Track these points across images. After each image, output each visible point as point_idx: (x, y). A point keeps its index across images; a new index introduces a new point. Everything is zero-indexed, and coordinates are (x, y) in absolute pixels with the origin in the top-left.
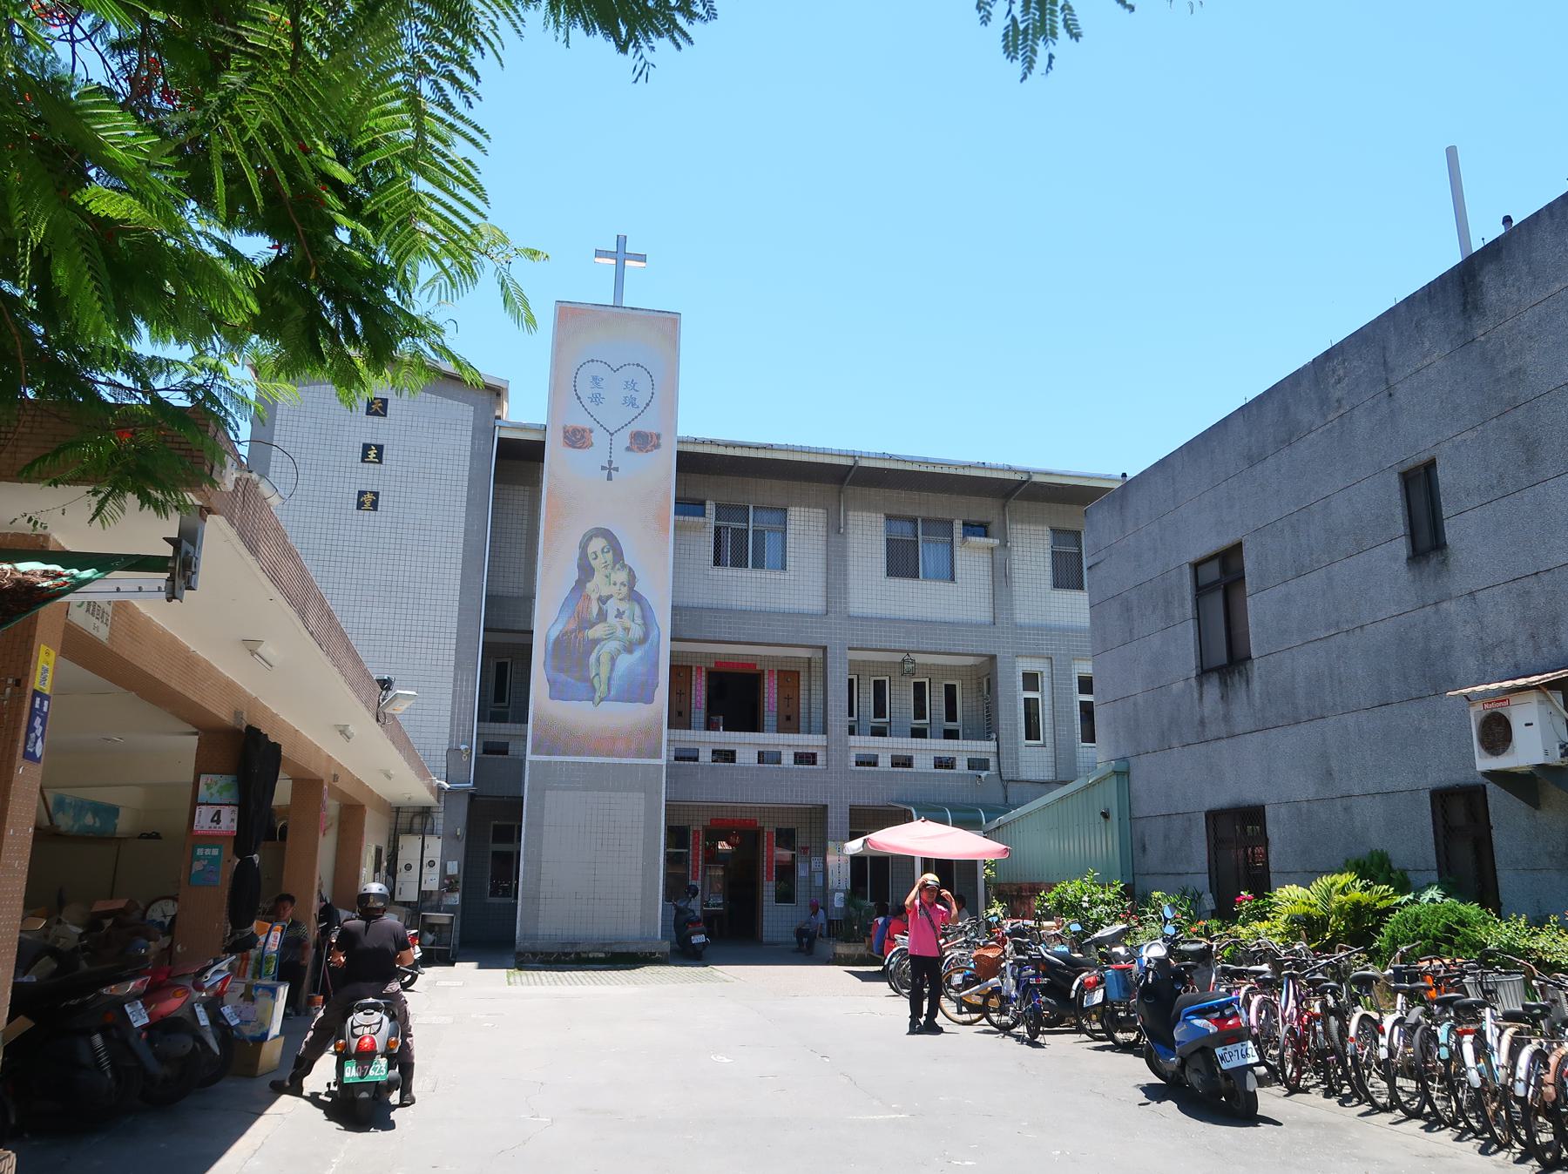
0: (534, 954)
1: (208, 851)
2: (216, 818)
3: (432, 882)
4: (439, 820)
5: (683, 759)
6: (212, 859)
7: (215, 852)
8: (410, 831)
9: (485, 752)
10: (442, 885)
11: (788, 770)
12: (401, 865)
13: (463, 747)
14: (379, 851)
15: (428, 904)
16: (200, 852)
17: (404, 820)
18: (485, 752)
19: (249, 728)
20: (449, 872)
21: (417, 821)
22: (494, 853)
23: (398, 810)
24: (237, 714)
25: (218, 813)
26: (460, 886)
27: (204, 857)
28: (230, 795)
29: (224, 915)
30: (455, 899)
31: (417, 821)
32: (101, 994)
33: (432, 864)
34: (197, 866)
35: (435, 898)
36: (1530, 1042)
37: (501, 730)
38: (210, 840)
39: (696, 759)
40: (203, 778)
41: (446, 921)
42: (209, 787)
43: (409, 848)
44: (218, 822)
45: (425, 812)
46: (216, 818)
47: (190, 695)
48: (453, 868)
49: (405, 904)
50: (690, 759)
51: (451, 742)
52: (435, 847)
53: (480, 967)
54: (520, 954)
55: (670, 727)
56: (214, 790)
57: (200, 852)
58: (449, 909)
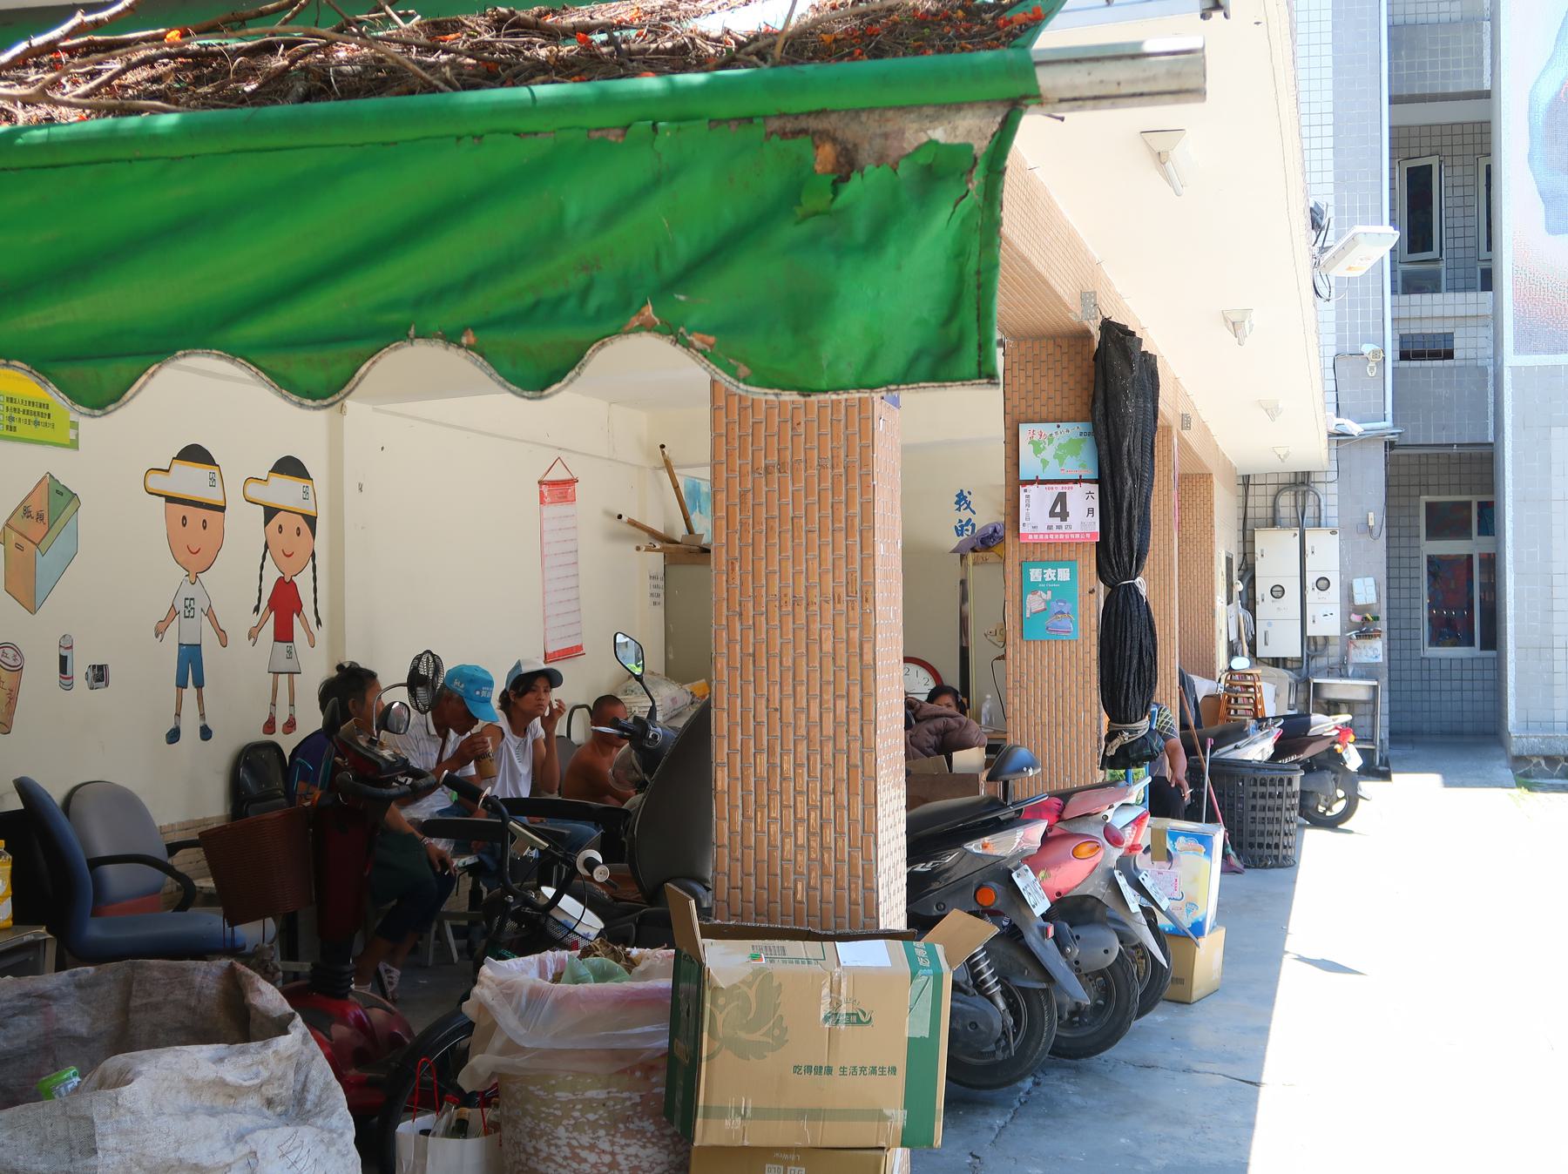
0: (1551, 760)
1: (1050, 574)
2: (1060, 509)
3: (1327, 620)
4: (1329, 496)
5: (1419, 356)
6: (1059, 589)
7: (1064, 574)
8: (1274, 522)
9: (1404, 356)
10: (1347, 626)
12: (1262, 588)
13: (1367, 349)
14: (1229, 561)
15: (1321, 662)
16: (1035, 574)
17: (1260, 502)
18: (1404, 356)
19: (1108, 326)
20: (1360, 600)
21: (1286, 501)
22: (1431, 560)
23: (1246, 481)
24: (1088, 298)
25: (1062, 498)
26: (1383, 626)
27: (1044, 586)
28: (1082, 462)
29: (1095, 696)
30: (1374, 651)
31: (1286, 501)
32: (967, 851)
33: (1278, 592)
34: (1034, 603)
35: (1334, 650)
36: (412, 822)
37: (1438, 310)
38: (1053, 552)
39: (1449, 355)
40: (1025, 430)
41: (1363, 695)
42: (1037, 449)
43: (1276, 555)
44: (1064, 515)
45: (1301, 482)
46: (1060, 509)
47: (1034, 261)
48: (1367, 592)
49: (1277, 662)
50: (1435, 355)
51: (1340, 340)
52: (1326, 552)
53: (1447, 784)
54: (1519, 759)
55: (1394, 292)
56: (1049, 452)
57: (1035, 574)
58: (1367, 672)
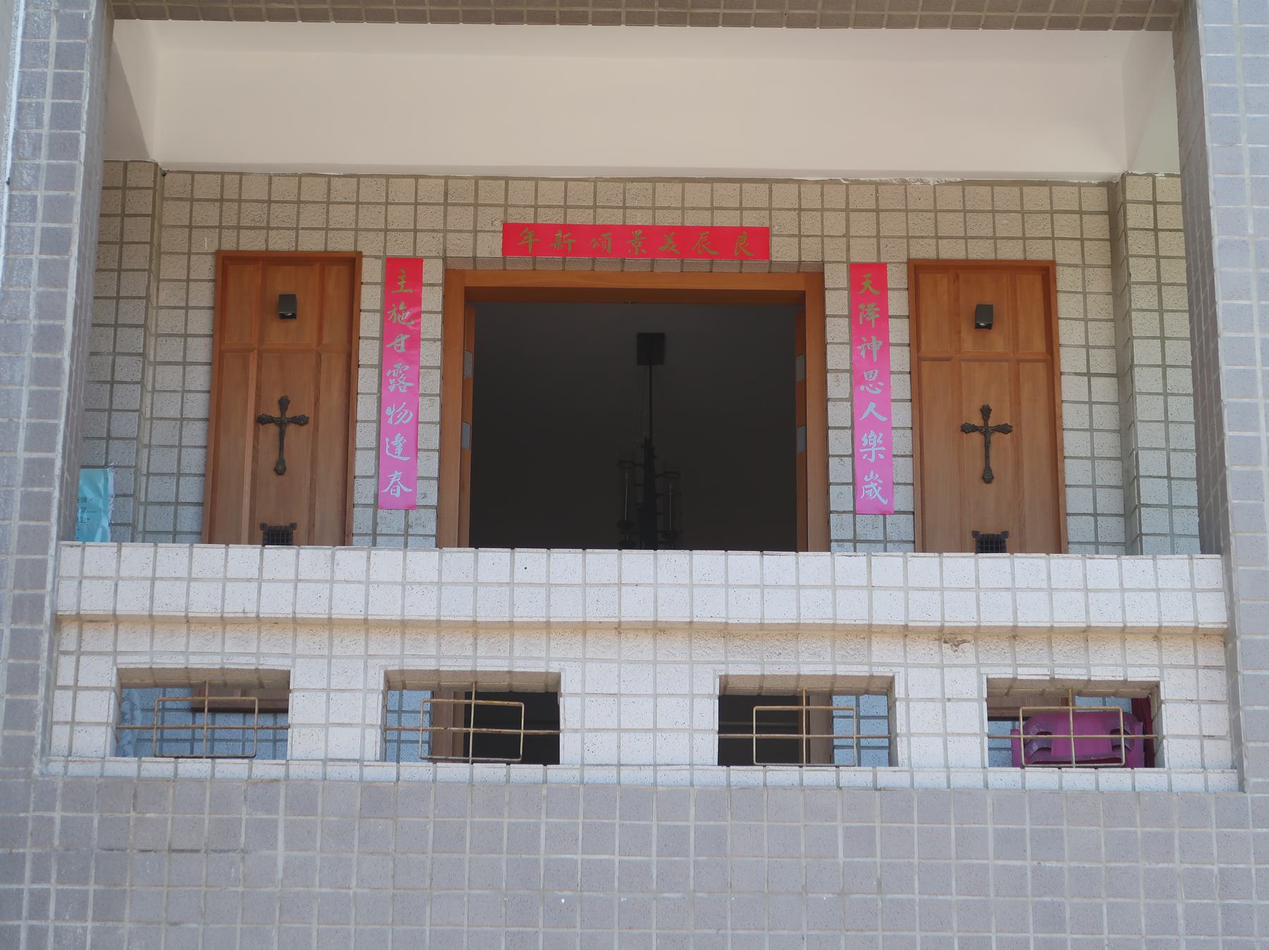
11: (939, 802)
